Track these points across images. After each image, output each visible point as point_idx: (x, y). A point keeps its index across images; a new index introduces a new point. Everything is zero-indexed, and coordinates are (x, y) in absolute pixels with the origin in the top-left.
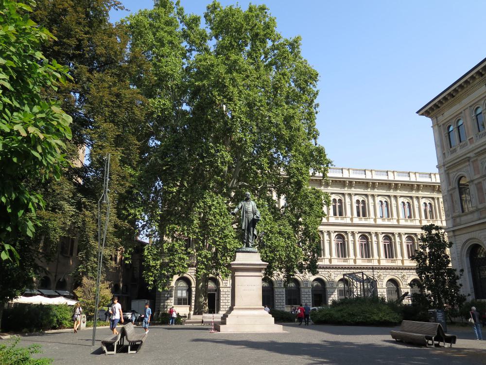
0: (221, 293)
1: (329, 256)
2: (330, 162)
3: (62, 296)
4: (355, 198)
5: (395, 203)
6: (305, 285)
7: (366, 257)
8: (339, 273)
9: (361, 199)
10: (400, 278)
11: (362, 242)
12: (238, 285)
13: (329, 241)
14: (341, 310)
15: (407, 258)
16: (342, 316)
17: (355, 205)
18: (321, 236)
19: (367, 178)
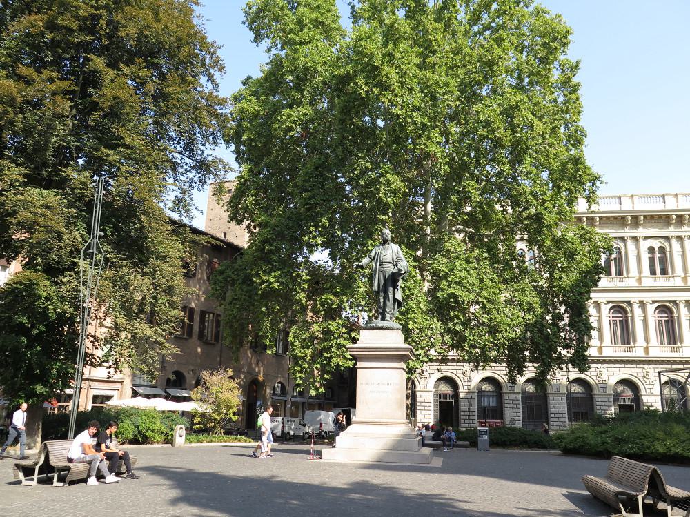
0: (418, 400)
1: (602, 343)
2: (597, 178)
3: (141, 395)
4: (644, 245)
5: (681, 249)
6: (601, 390)
7: (623, 343)
8: (617, 370)
9: (656, 245)
10: (641, 378)
11: (661, 317)
12: (362, 384)
13: (642, 318)
14: (605, 432)
15: (610, 344)
16: (604, 443)
17: (645, 257)
18: (628, 309)
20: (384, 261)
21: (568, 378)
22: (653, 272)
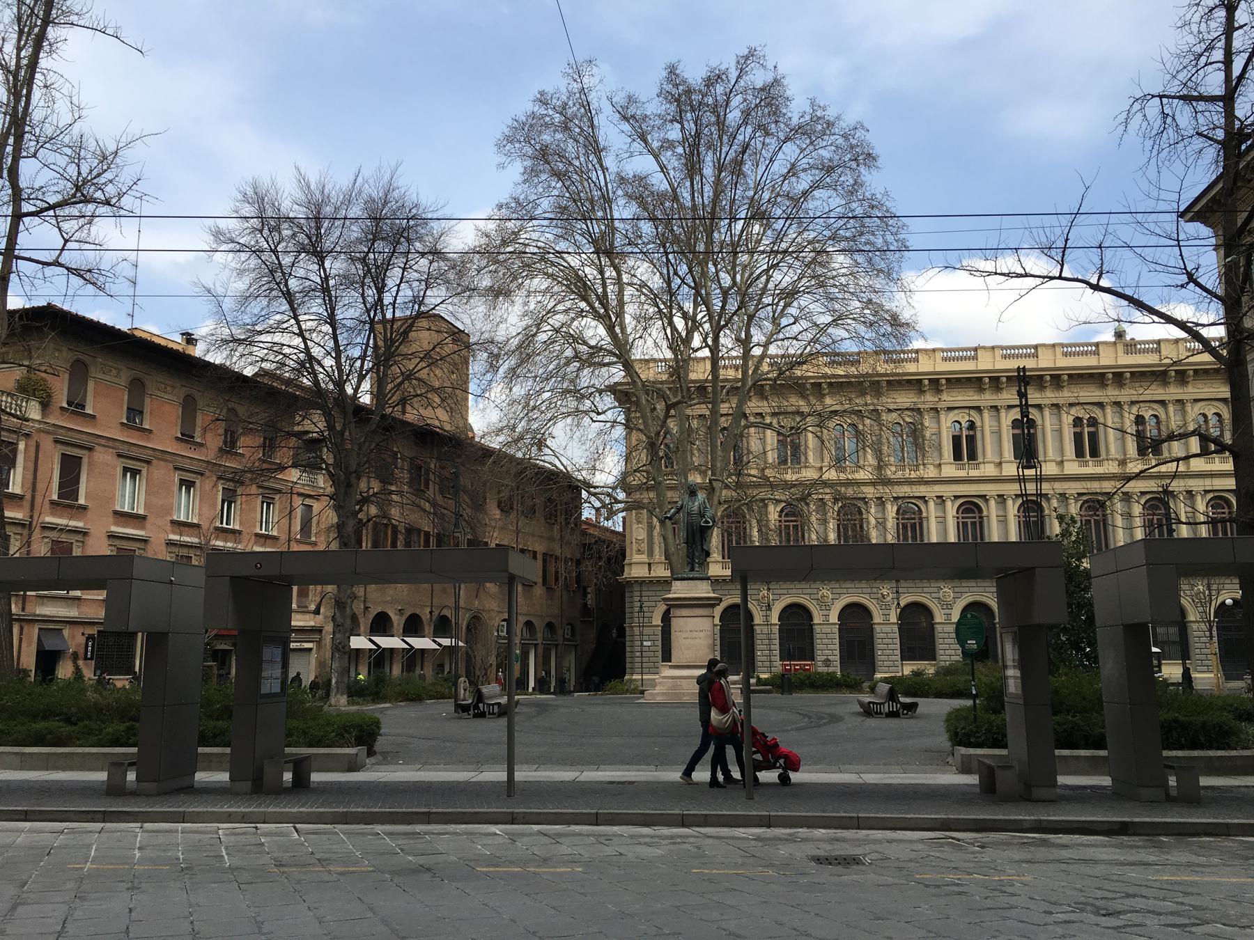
0: (758, 637)
18: (923, 508)
19: (1040, 366)
20: (548, 442)
21: (898, 604)
22: (1079, 453)
